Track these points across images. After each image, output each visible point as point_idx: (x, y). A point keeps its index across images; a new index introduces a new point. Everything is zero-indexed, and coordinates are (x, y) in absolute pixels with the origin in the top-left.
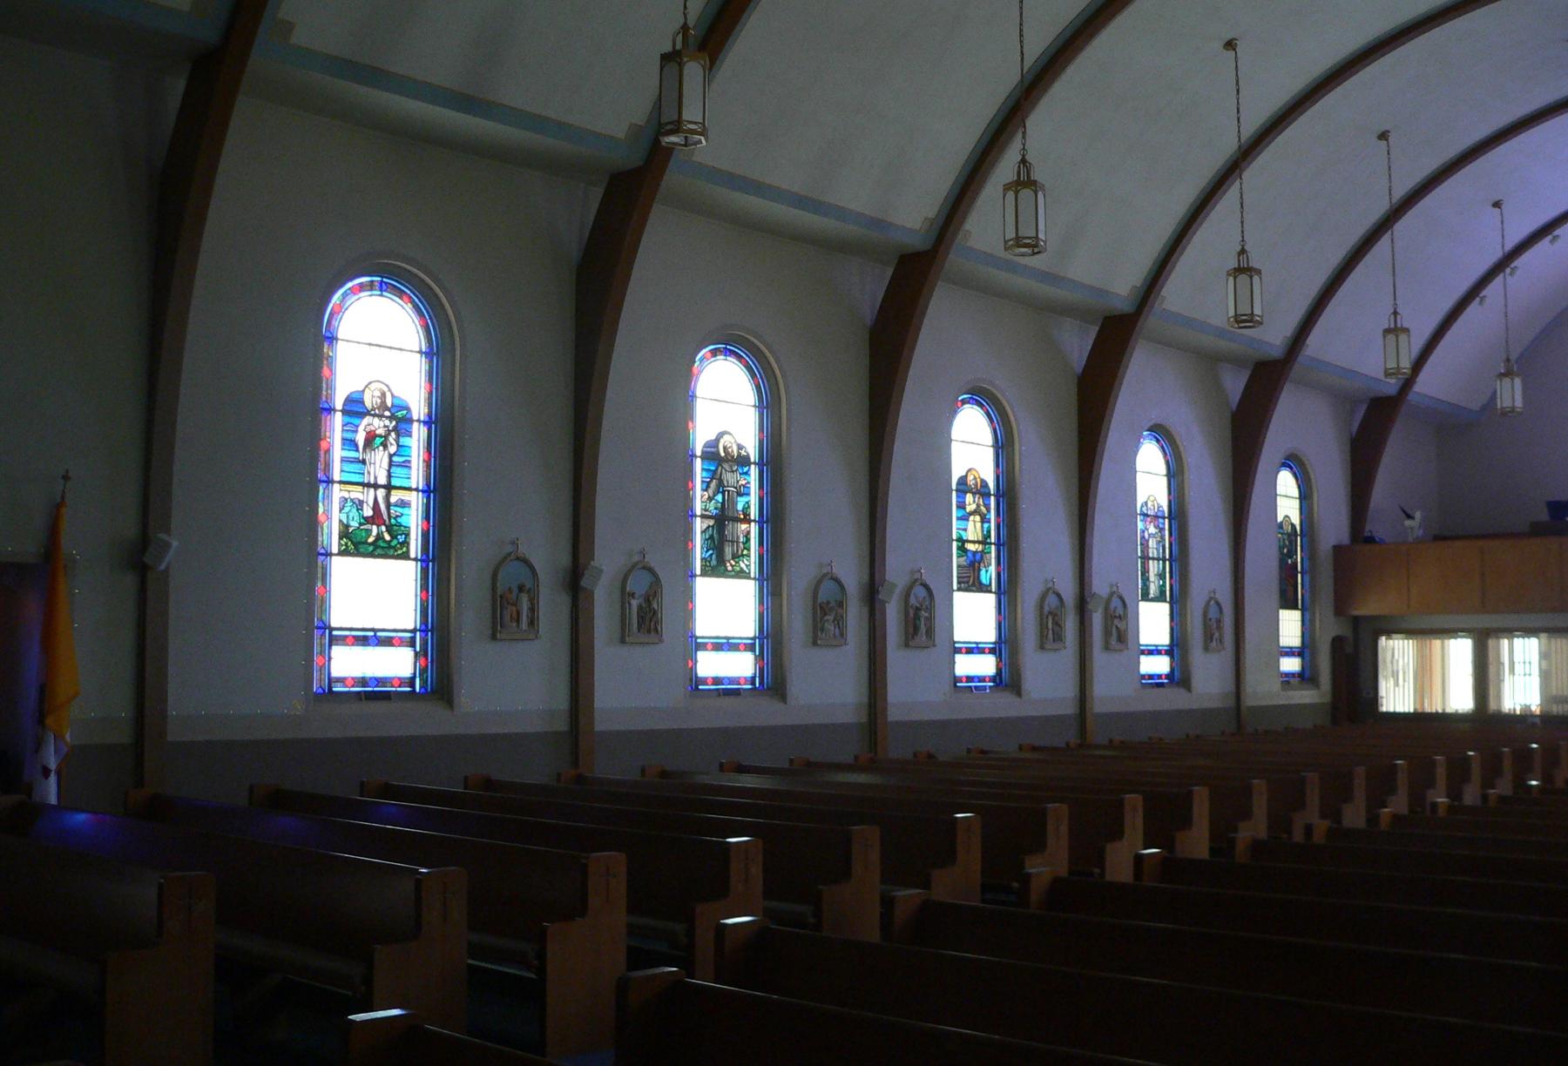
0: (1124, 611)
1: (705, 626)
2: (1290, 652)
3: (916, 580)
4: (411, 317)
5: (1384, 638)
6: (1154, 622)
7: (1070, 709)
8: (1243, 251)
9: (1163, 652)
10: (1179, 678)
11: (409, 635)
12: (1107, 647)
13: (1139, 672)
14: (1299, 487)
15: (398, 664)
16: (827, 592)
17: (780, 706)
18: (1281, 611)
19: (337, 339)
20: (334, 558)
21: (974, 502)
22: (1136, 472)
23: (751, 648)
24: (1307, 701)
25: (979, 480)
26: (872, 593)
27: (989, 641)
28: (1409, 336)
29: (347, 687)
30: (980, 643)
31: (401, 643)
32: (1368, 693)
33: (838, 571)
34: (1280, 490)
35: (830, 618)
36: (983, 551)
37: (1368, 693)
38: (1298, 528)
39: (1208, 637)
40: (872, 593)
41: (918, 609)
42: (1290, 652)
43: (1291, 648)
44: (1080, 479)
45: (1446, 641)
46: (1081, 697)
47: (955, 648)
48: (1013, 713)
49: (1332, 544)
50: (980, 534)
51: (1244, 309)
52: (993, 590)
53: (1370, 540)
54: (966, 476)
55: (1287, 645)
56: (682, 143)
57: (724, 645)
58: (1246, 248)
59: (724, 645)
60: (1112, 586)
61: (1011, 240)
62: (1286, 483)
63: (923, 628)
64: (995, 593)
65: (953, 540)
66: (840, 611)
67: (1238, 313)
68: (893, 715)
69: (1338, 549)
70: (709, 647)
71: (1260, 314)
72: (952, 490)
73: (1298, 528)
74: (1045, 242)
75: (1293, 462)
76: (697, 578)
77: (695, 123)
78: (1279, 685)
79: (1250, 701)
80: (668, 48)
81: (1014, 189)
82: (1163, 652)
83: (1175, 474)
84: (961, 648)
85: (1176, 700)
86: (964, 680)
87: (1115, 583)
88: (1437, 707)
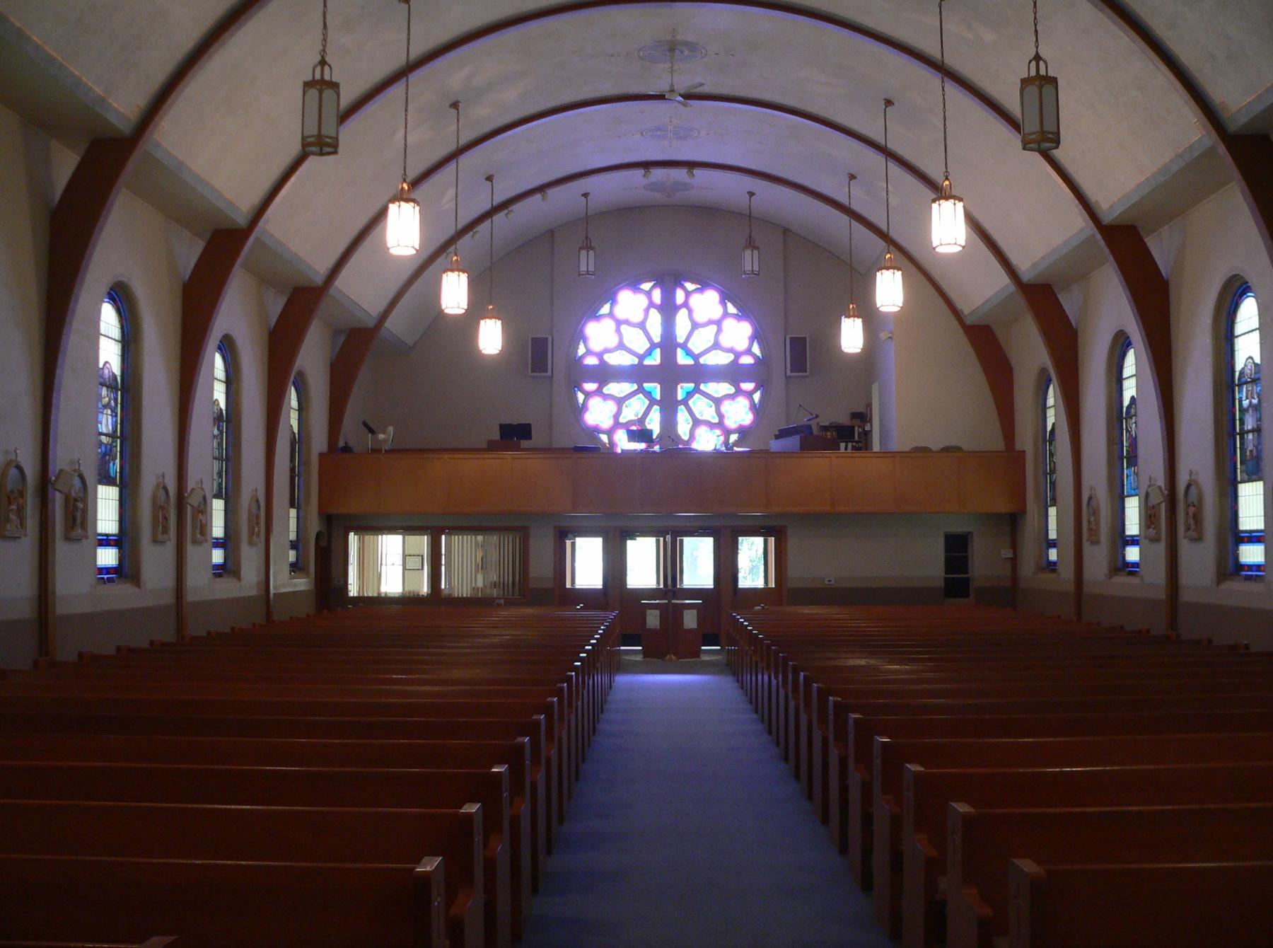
0: (84, 493)
2: (105, 541)
3: (11, 462)
5: (353, 533)
9: (1246, 568)
10: (126, 571)
12: (67, 538)
13: (96, 564)
14: (122, 328)
17: (136, 590)
18: (214, 500)
21: (107, 396)
24: (350, 587)
25: (111, 374)
32: (339, 581)
35: (14, 507)
36: (111, 445)
37: (339, 581)
38: (224, 412)
39: (251, 533)
41: (76, 500)
42: (105, 541)
43: (107, 535)
44: (182, 384)
45: (367, 537)
46: (40, 597)
48: (236, 594)
50: (110, 428)
52: (118, 483)
53: (347, 449)
55: (104, 532)
60: (7, 453)
61: (312, 136)
62: (109, 317)
63: (79, 520)
66: (21, 501)
68: (61, 609)
69: (321, 455)
73: (224, 412)
75: (121, 297)
78: (210, 575)
80: (309, 78)
82: (1246, 568)
83: (130, 341)
85: (122, 596)
87: (76, 459)
88: (370, 593)
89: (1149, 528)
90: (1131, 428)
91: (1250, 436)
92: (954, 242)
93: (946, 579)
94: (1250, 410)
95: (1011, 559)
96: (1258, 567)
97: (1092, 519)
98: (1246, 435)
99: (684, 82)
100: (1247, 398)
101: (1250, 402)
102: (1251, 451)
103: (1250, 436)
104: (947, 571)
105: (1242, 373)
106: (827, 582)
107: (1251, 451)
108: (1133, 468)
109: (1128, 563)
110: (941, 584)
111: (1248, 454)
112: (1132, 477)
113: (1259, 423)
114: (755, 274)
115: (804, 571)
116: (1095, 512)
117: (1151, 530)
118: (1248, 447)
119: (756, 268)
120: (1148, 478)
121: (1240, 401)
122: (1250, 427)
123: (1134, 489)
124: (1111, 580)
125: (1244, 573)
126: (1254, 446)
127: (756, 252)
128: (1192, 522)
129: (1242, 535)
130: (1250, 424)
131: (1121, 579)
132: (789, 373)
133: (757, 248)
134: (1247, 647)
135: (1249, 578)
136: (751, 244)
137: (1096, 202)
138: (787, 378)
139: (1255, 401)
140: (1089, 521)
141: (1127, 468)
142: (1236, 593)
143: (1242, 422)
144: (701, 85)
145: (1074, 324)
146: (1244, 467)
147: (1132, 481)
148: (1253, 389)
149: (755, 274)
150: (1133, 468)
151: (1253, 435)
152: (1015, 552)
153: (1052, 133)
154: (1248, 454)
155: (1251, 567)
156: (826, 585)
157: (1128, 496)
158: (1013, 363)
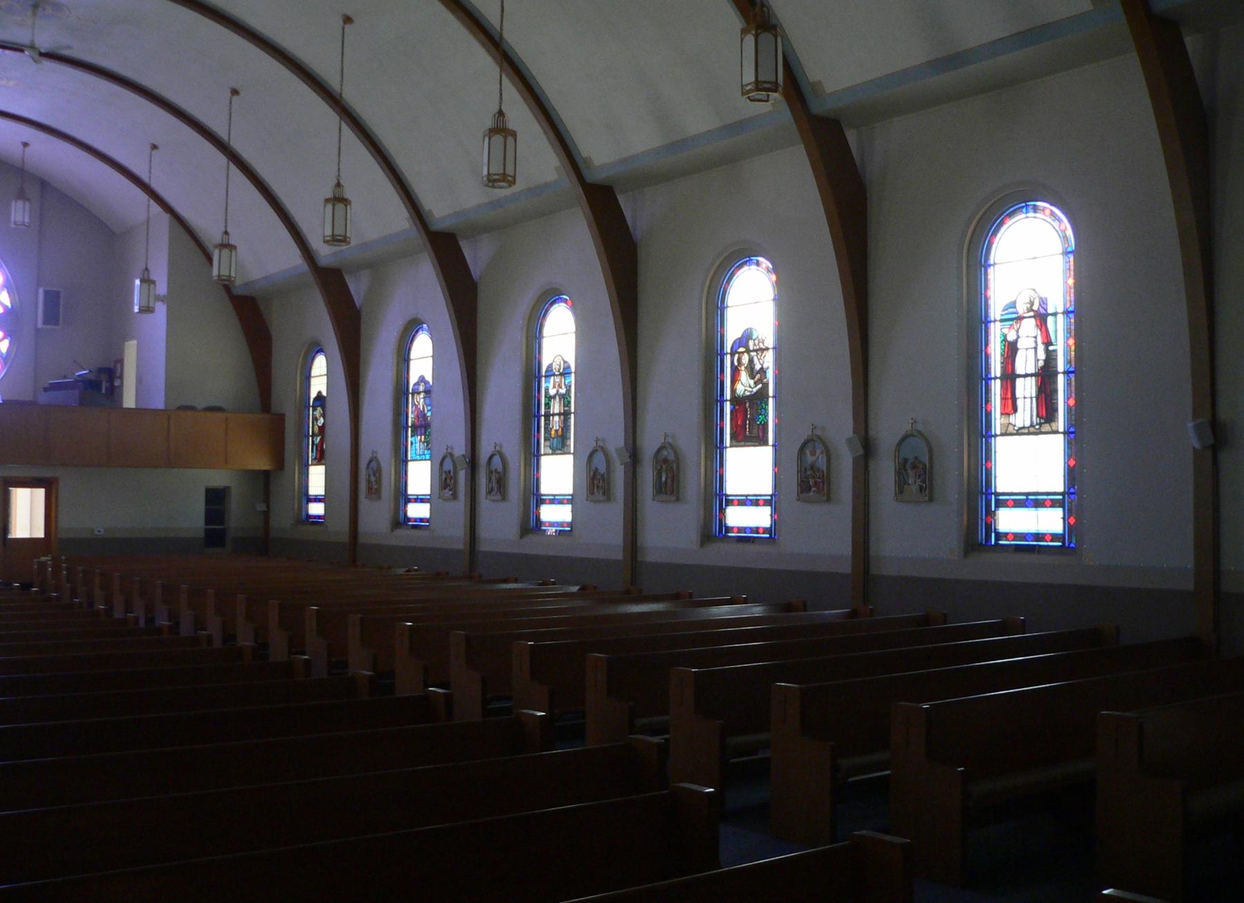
1: (733, 486)
2: (317, 499)
4: (1005, 231)
6: (420, 477)
7: (345, 538)
8: (338, 185)
9: (556, 524)
11: (1061, 497)
15: (1051, 521)
16: (448, 465)
19: (1063, 254)
20: (998, 438)
22: (575, 333)
23: (569, 501)
26: (866, 448)
27: (567, 493)
28: (155, 286)
29: (1008, 540)
30: (749, 495)
31: (1054, 504)
33: (505, 450)
34: (314, 372)
40: (866, 448)
47: (541, 499)
49: (287, 414)
51: (339, 231)
54: (552, 364)
56: (773, 88)
57: (555, 500)
58: (341, 182)
59: (555, 500)
60: (373, 452)
61: (750, 84)
64: (573, 454)
65: (574, 413)
67: (760, 78)
70: (736, 502)
71: (234, 276)
72: (575, 373)
74: (235, 278)
76: (728, 450)
77: (340, 236)
79: (483, 547)
81: (753, 32)
84: (733, 500)
86: (735, 530)
89: (445, 489)
90: (419, 403)
91: (556, 418)
92: (1028, 351)
93: (206, 530)
94: (557, 397)
95: (265, 512)
96: (319, 517)
97: (373, 479)
98: (551, 417)
99: (45, 41)
100: (554, 387)
101: (558, 391)
102: (556, 431)
103: (556, 418)
104: (208, 522)
105: (550, 367)
106: (96, 533)
107: (556, 431)
108: (419, 437)
109: (310, 516)
110: (202, 534)
111: (553, 432)
112: (418, 445)
113: (566, 408)
114: (26, 226)
115: (77, 522)
116: (377, 472)
117: (447, 490)
118: (553, 427)
119: (27, 220)
120: (446, 447)
121: (547, 389)
122: (557, 411)
123: (420, 455)
124: (394, 533)
125: (410, 523)
126: (559, 427)
127: (27, 204)
128: (495, 486)
129: (544, 497)
130: (556, 407)
131: (399, 532)
132: (40, 325)
133: (28, 200)
134: (595, 587)
135: (414, 527)
136: (21, 195)
137: (430, 211)
138: (37, 331)
139: (563, 391)
140: (369, 482)
141: (412, 436)
142: (402, 538)
143: (548, 405)
144: (69, 47)
145: (358, 307)
146: (548, 443)
147: (418, 448)
148: (561, 381)
149: (26, 226)
150: (419, 437)
151: (560, 418)
152: (268, 507)
153: (511, 176)
154: (553, 432)
155: (315, 517)
156: (96, 535)
157: (412, 460)
158: (273, 333)
